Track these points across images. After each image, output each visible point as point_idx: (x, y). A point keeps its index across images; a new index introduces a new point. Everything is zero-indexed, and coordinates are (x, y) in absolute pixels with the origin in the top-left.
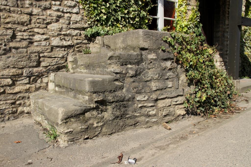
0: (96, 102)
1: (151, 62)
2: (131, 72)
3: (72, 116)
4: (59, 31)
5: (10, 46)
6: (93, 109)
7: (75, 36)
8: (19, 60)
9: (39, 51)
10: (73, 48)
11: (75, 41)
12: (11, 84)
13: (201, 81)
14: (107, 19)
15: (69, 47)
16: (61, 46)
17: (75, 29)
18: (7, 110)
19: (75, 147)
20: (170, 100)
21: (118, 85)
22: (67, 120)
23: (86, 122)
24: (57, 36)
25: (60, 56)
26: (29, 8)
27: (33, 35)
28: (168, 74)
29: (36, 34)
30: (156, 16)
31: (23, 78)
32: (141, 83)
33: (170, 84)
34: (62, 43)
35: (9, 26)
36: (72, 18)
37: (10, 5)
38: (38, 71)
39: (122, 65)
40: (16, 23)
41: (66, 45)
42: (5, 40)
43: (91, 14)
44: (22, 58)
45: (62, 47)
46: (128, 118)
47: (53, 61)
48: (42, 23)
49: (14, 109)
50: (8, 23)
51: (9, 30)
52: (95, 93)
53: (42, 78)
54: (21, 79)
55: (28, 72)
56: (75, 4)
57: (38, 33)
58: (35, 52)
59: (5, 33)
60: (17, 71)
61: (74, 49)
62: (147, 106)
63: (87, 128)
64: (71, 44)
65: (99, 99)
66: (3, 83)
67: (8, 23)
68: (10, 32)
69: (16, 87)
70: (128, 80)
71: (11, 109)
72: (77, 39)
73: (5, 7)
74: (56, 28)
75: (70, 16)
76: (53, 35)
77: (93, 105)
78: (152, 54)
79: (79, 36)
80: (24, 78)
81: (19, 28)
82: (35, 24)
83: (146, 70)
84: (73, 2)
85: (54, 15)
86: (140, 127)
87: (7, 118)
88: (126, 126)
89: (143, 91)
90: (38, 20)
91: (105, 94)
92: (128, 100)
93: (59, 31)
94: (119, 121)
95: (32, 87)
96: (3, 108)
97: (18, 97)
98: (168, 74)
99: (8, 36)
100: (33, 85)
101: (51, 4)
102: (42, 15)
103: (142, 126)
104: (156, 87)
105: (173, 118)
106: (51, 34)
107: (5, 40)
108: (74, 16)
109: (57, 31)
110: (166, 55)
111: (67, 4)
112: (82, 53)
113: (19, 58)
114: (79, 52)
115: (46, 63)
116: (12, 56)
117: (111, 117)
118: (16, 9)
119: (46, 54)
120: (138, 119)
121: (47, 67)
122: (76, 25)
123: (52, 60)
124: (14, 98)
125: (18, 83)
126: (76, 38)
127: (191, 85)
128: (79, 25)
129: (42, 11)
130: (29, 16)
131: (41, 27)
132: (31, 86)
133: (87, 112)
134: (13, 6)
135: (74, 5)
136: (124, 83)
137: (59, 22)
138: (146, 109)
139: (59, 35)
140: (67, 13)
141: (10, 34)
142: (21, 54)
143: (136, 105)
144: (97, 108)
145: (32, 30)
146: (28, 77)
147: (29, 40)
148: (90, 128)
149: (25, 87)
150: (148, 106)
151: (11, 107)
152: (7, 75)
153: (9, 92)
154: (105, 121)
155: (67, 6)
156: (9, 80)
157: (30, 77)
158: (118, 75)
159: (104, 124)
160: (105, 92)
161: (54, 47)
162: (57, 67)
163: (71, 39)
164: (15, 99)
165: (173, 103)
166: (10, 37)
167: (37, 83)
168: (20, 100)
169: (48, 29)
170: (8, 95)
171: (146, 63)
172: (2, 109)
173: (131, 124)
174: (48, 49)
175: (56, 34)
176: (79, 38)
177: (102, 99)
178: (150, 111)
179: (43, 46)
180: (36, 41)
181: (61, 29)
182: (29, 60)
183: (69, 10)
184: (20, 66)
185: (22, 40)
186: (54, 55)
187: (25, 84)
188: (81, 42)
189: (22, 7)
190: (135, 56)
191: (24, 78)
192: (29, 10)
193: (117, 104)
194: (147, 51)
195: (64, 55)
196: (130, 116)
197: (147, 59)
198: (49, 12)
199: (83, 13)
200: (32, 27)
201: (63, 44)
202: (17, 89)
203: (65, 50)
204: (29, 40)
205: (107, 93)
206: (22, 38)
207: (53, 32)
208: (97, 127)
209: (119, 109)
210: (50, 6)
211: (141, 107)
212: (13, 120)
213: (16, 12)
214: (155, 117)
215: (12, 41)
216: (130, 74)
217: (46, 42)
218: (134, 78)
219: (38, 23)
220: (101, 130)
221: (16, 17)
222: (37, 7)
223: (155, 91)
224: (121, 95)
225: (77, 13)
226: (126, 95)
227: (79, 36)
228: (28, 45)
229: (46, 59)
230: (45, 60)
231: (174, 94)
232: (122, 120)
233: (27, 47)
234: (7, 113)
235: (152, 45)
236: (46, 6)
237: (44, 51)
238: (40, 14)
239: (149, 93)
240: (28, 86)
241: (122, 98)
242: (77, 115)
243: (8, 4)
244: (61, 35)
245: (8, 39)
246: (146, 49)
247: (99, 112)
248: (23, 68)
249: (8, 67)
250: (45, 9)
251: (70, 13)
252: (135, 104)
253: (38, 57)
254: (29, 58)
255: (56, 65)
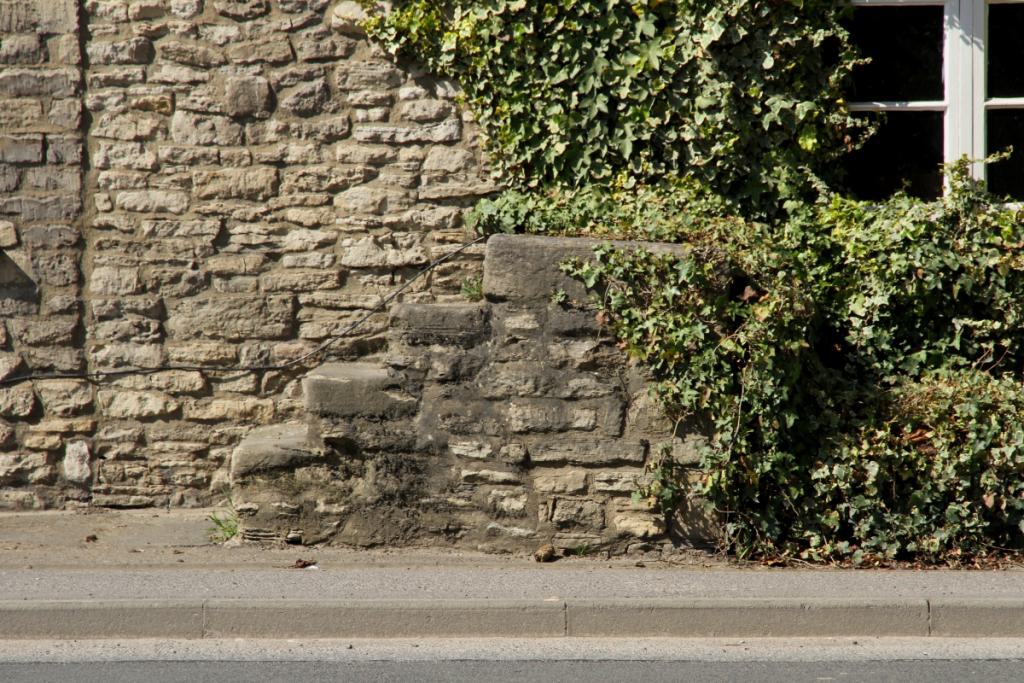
0: (329, 442)
1: (515, 340)
2: (440, 368)
3: (259, 470)
4: (373, 213)
5: (209, 269)
6: (318, 460)
7: (437, 228)
8: (231, 312)
9: (296, 285)
10: (425, 274)
11: (435, 250)
12: (200, 390)
13: (713, 418)
14: (569, 160)
15: (409, 270)
16: (377, 267)
17: (439, 201)
18: (179, 473)
19: (254, 553)
20: (581, 473)
21: (397, 403)
22: (246, 479)
23: (297, 493)
24: (366, 232)
25: (371, 304)
26: (276, 142)
27: (283, 232)
28: (574, 383)
29: (293, 226)
30: (941, 97)
31: (238, 373)
32: (473, 405)
33: (582, 417)
34: (382, 254)
35: (213, 205)
36: (427, 161)
37: (222, 143)
38: (288, 353)
39: (414, 344)
40: (234, 194)
41: (398, 261)
42: (197, 251)
43: (502, 142)
44: (241, 306)
45: (382, 270)
46: (426, 508)
47: (344, 321)
48: (314, 189)
49: (201, 474)
50: (210, 197)
51: (211, 218)
52: (324, 415)
53: (299, 380)
54: (231, 376)
55: (254, 354)
56: (444, 108)
57: (300, 224)
58: (283, 289)
59: (197, 230)
60: (222, 350)
61: (430, 279)
62: (490, 479)
63: (297, 511)
64: (418, 259)
65: (334, 435)
66: (176, 384)
67: (210, 197)
68: (212, 223)
69: (215, 402)
70: (433, 391)
71: (192, 471)
72: (442, 241)
73: (206, 149)
74: (361, 202)
75: (421, 156)
76: (350, 228)
77: (319, 450)
78: (521, 314)
79: (454, 227)
80: (242, 373)
81: (241, 209)
82: (291, 192)
83: (492, 364)
84: (434, 100)
85: (359, 159)
86: (468, 544)
87: (176, 497)
88: (421, 533)
89: (476, 429)
90: (301, 180)
91: (353, 424)
92: (427, 450)
93: (373, 213)
94: (397, 509)
95: (263, 408)
96: (171, 464)
97: (216, 434)
98: (574, 383)
99: (204, 238)
100: (269, 402)
101: (349, 120)
102: (315, 163)
103: (475, 543)
104: (524, 421)
105: (598, 541)
106: (342, 225)
107: (197, 251)
108: (436, 156)
109: (367, 213)
110: (569, 320)
111: (412, 113)
112: (458, 296)
113: (230, 308)
114: (448, 288)
115: (316, 326)
116: (211, 299)
117: (372, 494)
118: (236, 151)
119: (318, 296)
120: (463, 517)
121: (319, 340)
122: (443, 186)
123: (340, 318)
124: (205, 436)
125: (222, 387)
126: (438, 235)
127: (690, 433)
128: (457, 185)
129: (318, 148)
130: (273, 170)
131: (310, 202)
132: (262, 402)
133: (300, 465)
134: (228, 145)
135: (438, 114)
136: (421, 399)
137: (375, 181)
138: (487, 488)
139: (369, 228)
140: (408, 144)
141: (211, 231)
142: (239, 295)
143: (453, 470)
144: (329, 460)
145: (280, 214)
146: (254, 371)
147: (265, 249)
148: (306, 514)
149: (242, 403)
150: (495, 479)
151: (192, 464)
152: (191, 361)
153: (192, 416)
154: (355, 502)
155: (410, 120)
156: (196, 375)
157: (259, 372)
158: (402, 374)
159: (349, 512)
160: (353, 416)
161: (352, 272)
162: (355, 344)
163: (418, 240)
164: (206, 441)
165: (596, 484)
166: (212, 242)
167: (283, 395)
168: (221, 445)
169: (335, 208)
170: (190, 424)
171: (495, 343)
172: (167, 467)
173: (433, 528)
174: (327, 276)
175: (362, 225)
176: (450, 238)
177: (341, 434)
178: (502, 499)
179: (313, 267)
180: (291, 252)
181: (380, 204)
182: (260, 313)
183: (419, 133)
184: (233, 333)
185: (247, 250)
186: (349, 299)
187: (242, 392)
188: (458, 253)
189: (256, 143)
190: (461, 318)
191: (242, 373)
192: (274, 152)
193: (390, 456)
194: (506, 304)
195: (385, 298)
196: (432, 500)
197: (502, 329)
198: (340, 149)
199: (475, 138)
200: (279, 205)
201: (384, 259)
202: (215, 408)
203: (392, 283)
204: (265, 249)
205: (362, 421)
206: (245, 241)
207: (352, 219)
208: (327, 514)
209: (396, 472)
210: (347, 128)
211: (470, 479)
212: (193, 507)
213: (236, 160)
214: (524, 522)
215: (216, 252)
216: (437, 372)
217: (321, 255)
218: (451, 387)
219: (301, 190)
220: (339, 526)
221: (234, 176)
222: (304, 137)
223: (520, 433)
224: (402, 433)
225: (449, 142)
226: (418, 433)
227: (454, 227)
228: (262, 264)
229: (318, 312)
230: (314, 318)
231: (598, 454)
232: (406, 509)
233: (257, 272)
234: (179, 482)
235: (519, 287)
236: (333, 130)
237: (312, 286)
238: (310, 160)
239: (496, 436)
240: (251, 401)
241: (405, 442)
242: (272, 469)
243: (215, 141)
244: (380, 225)
245: (203, 248)
246: (502, 299)
247: (338, 473)
248: (239, 341)
249: (198, 334)
250: (331, 139)
251: (420, 143)
252: (450, 466)
253: (289, 305)
254: (261, 308)
255: (351, 335)
